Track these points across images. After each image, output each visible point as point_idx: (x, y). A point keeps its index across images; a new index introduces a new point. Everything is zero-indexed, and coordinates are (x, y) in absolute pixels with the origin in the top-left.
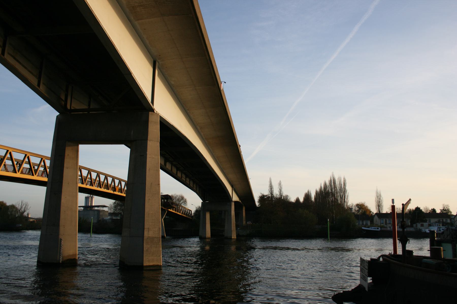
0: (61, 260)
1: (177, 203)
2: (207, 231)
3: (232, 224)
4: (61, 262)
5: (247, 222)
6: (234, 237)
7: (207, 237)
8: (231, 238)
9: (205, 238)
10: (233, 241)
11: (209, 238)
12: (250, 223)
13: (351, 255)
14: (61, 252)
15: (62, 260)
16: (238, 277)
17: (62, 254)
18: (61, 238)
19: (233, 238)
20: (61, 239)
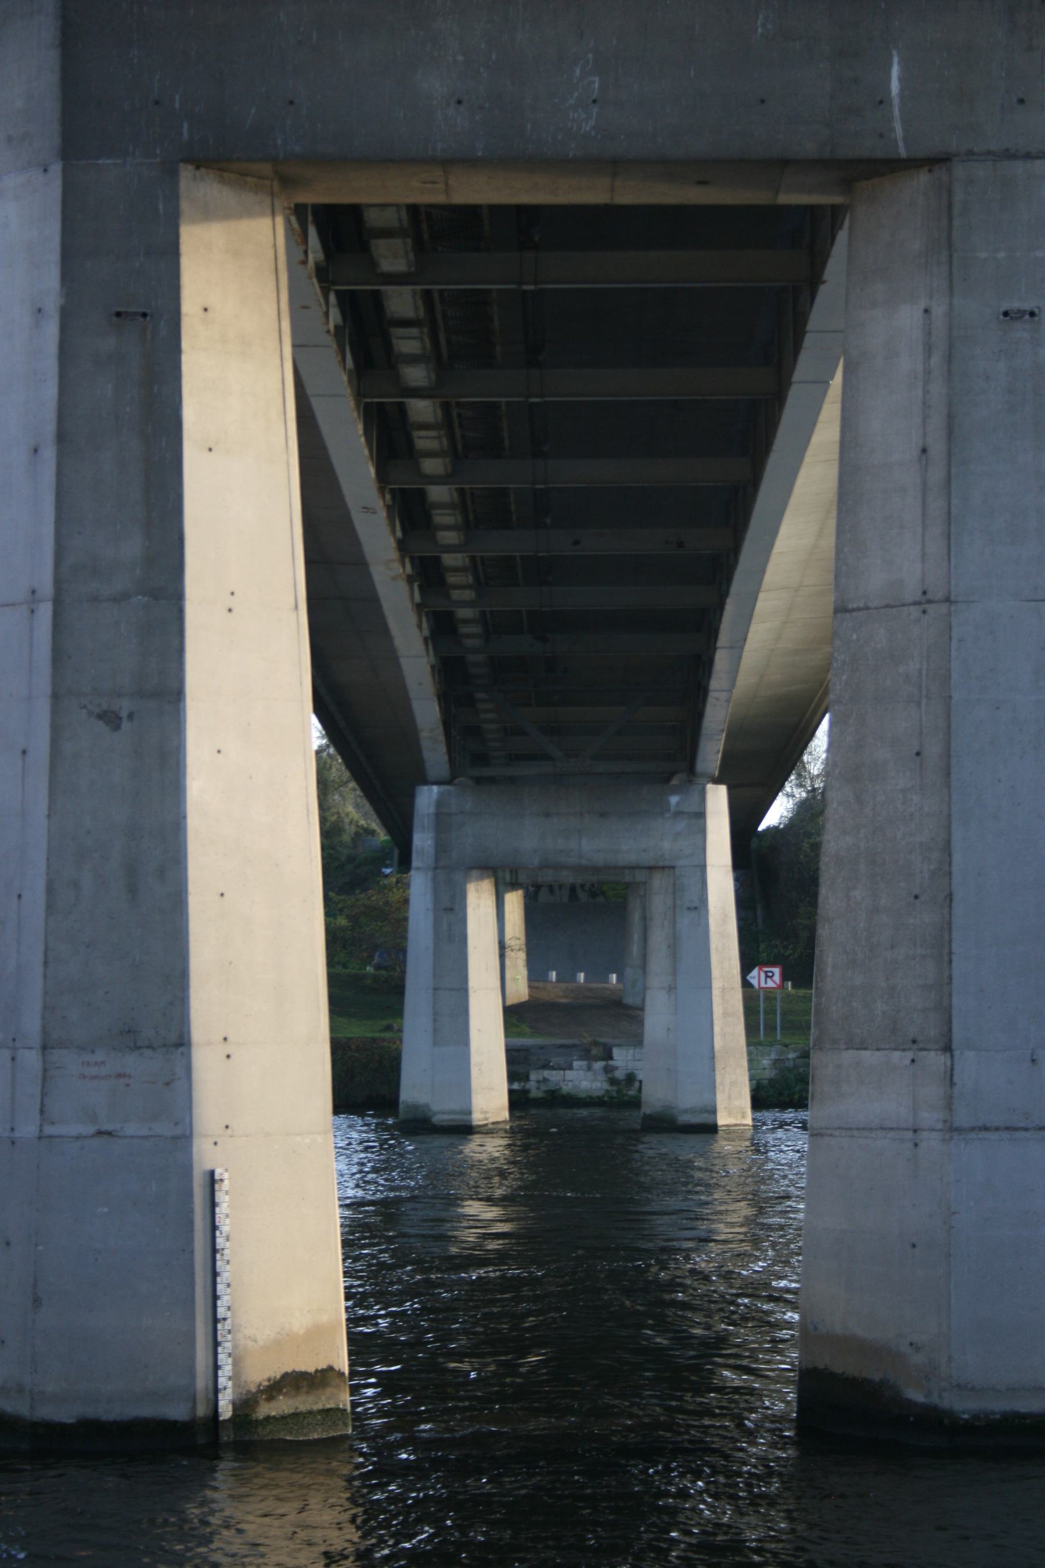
0: (230, 1384)
1: (339, 797)
2: (474, 1059)
3: (716, 993)
4: (226, 1411)
5: (750, 970)
6: (730, 1114)
7: (477, 1118)
8: (711, 1129)
9: (465, 1130)
10: (724, 1146)
11: (487, 1130)
12: (777, 978)
13: (772, 1237)
14: (221, 1312)
15: (234, 1385)
16: (871, 1495)
17: (228, 1325)
18: (209, 1167)
19: (723, 1120)
20: (212, 1180)
